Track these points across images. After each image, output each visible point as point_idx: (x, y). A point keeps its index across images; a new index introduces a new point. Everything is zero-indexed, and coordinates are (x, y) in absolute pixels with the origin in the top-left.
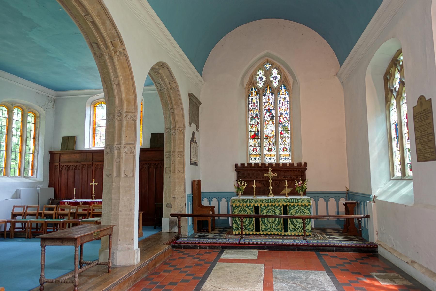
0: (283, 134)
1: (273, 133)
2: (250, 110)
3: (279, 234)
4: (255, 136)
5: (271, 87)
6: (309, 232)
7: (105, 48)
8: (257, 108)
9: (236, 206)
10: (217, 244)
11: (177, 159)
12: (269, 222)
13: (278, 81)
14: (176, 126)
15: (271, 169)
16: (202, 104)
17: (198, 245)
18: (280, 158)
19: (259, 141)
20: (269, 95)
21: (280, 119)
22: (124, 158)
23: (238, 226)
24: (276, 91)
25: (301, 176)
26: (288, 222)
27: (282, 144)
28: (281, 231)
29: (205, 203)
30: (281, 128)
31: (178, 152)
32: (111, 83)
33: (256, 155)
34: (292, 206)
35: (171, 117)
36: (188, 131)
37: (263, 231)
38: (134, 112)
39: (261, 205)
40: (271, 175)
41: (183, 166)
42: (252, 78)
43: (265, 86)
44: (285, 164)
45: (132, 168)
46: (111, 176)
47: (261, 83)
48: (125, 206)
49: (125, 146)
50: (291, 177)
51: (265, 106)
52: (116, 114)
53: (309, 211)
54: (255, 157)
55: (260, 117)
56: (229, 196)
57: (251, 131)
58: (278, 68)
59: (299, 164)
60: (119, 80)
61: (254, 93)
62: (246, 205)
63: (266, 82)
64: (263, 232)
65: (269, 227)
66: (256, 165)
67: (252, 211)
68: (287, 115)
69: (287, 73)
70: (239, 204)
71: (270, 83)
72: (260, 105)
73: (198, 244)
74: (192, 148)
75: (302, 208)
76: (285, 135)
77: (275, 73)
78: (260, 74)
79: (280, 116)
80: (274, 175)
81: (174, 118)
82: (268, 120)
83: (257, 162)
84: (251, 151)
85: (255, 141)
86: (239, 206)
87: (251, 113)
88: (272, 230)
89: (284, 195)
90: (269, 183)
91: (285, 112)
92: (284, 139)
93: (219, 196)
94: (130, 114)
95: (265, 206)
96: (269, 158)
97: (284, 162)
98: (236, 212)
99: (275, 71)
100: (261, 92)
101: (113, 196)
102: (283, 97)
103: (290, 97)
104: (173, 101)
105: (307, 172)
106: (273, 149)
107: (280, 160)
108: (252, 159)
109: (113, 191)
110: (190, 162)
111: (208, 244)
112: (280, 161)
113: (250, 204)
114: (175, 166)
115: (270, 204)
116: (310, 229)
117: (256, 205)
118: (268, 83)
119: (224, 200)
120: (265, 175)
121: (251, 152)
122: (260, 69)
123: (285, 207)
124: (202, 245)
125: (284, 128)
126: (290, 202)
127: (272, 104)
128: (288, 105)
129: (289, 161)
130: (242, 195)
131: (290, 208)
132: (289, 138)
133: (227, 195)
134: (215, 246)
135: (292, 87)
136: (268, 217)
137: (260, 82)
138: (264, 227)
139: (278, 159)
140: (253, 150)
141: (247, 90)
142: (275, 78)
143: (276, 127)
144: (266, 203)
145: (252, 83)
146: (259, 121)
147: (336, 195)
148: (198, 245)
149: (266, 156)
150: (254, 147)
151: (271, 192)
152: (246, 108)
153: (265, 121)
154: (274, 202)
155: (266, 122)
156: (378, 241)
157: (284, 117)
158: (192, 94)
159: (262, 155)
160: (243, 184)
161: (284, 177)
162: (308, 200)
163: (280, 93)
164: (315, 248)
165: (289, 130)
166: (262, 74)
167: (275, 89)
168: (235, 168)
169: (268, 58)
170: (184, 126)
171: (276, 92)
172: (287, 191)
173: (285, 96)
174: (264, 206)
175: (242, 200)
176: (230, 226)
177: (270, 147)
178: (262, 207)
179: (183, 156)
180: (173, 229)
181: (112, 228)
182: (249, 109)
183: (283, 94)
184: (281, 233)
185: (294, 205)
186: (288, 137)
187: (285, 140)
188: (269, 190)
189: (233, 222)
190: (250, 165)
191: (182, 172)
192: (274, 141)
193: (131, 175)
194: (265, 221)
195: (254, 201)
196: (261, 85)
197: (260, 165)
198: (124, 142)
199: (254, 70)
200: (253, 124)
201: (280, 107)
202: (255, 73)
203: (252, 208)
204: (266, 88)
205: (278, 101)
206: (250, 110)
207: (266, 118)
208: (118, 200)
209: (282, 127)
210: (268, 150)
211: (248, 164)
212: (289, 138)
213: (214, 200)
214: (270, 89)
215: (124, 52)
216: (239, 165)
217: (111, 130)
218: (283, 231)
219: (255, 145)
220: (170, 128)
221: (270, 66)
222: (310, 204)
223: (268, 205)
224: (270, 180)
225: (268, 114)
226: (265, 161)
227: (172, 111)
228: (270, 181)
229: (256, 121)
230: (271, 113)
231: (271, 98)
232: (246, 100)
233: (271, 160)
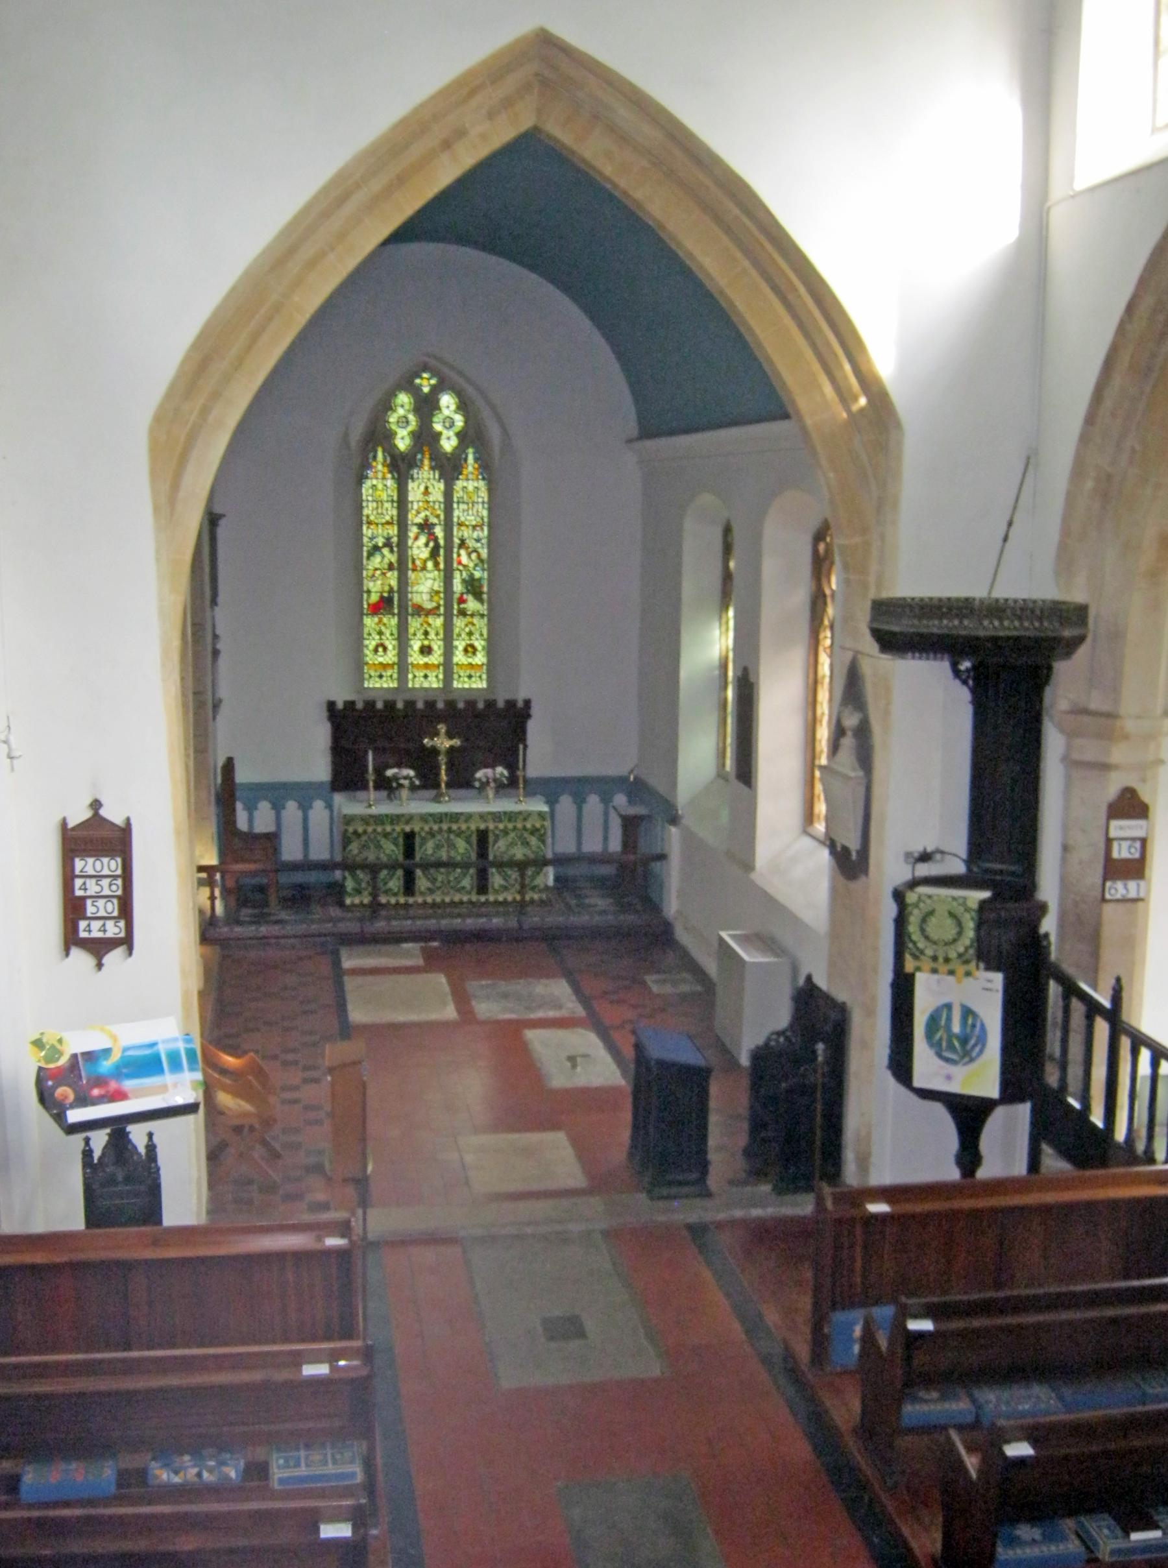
1: (436, 598)
4: (383, 605)
8: (388, 518)
9: (355, 833)
18: (456, 676)
19: (394, 621)
20: (429, 479)
21: (459, 555)
33: (385, 666)
37: (422, 893)
51: (414, 512)
59: (511, 704)
67: (396, 845)
68: (479, 545)
69: (486, 414)
85: (380, 621)
92: (469, 619)
93: (277, 793)
99: (447, 401)
100: (403, 466)
102: (470, 488)
103: (490, 491)
105: (532, 726)
106: (435, 647)
113: (393, 827)
115: (445, 826)
117: (408, 829)
118: (425, 438)
121: (370, 657)
123: (409, 837)
125: (472, 586)
127: (437, 507)
132: (482, 616)
140: (376, 651)
145: (378, 435)
147: (605, 786)
150: (379, 642)
153: (413, 561)
155: (418, 563)
157: (470, 550)
159: (448, 665)
166: (407, 407)
171: (449, 468)
173: (476, 484)
177: (426, 643)
185: (506, 827)
186: (481, 612)
187: (470, 620)
192: (438, 622)
196: (403, 443)
200: (376, 569)
202: (387, 406)
207: (415, 552)
209: (464, 581)
212: (482, 616)
213: (264, 807)
216: (340, 705)
219: (380, 633)
221: (433, 382)
230: (432, 537)
231: (434, 488)
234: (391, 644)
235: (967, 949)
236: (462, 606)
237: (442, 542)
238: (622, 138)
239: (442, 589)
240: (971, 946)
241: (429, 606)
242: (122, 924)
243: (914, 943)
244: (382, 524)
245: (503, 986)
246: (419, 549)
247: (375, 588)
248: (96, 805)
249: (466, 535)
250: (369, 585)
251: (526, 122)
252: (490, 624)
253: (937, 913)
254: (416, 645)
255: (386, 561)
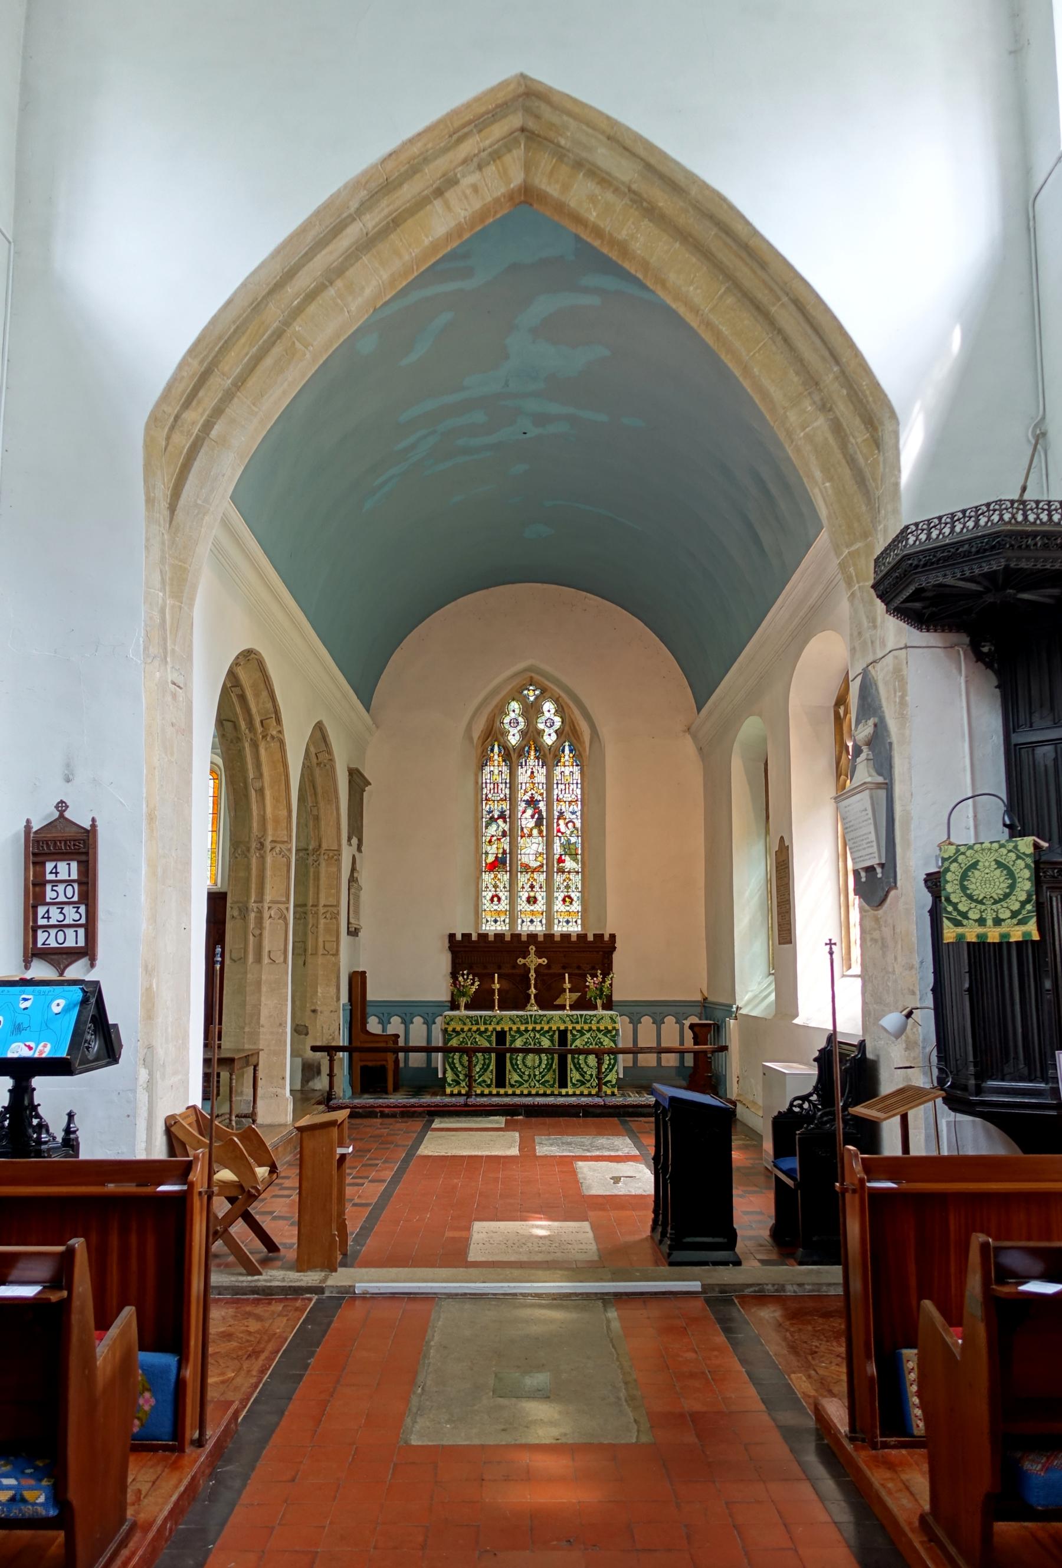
0: (563, 861)
1: (540, 859)
2: (486, 800)
3: (549, 1092)
5: (539, 744)
6: (613, 1086)
7: (247, 731)
8: (502, 796)
9: (454, 1030)
10: (418, 1107)
11: (322, 921)
12: (526, 1066)
13: (556, 732)
14: (320, 846)
15: (534, 949)
16: (370, 784)
17: (378, 1110)
18: (556, 921)
19: (507, 877)
20: (534, 766)
21: (558, 825)
22: (267, 928)
23: (458, 1076)
24: (550, 757)
25: (603, 964)
26: (569, 1066)
27: (562, 887)
28: (552, 1086)
29: (373, 1026)
30: (559, 848)
31: (325, 906)
32: (246, 787)
33: (498, 912)
34: (578, 1031)
35: (311, 824)
36: (347, 853)
37: (512, 1086)
38: (286, 842)
39: (510, 1029)
40: (533, 961)
41: (335, 939)
42: (493, 721)
43: (524, 743)
44: (566, 937)
45: (282, 947)
46: (243, 960)
47: (514, 735)
48: (270, 1016)
49: (270, 905)
50: (579, 968)
51: (522, 791)
52: (254, 845)
53: (614, 1042)
54: (495, 916)
55: (510, 817)
56: (431, 1010)
57: (487, 853)
58: (557, 701)
59: (599, 937)
60: (263, 782)
61: (496, 757)
62: (478, 1029)
63: (527, 733)
64: (513, 1089)
65: (526, 1078)
66: (499, 936)
68: (574, 816)
70: (462, 1026)
71: (537, 736)
72: (510, 788)
73: (377, 1107)
74: (351, 897)
75: (600, 1035)
76: (569, 864)
77: (549, 711)
78: (514, 711)
79: (559, 819)
80: (540, 961)
81: (317, 826)
82: (528, 825)
83: (499, 928)
84: (486, 902)
86: (462, 1030)
87: (488, 806)
88: (533, 1084)
89: (562, 1007)
90: (529, 980)
91: (571, 809)
92: (566, 875)
93: (407, 1010)
94: (278, 846)
95: (518, 1031)
96: (529, 920)
97: (565, 929)
98: (454, 1043)
99: (548, 707)
100: (514, 756)
101: (248, 998)
102: (567, 773)
104: (319, 791)
105: (616, 957)
106: (539, 898)
107: (556, 926)
108: (487, 921)
109: (248, 989)
110: (348, 928)
111: (399, 1107)
112: (556, 929)
114: (317, 939)
115: (530, 1027)
116: (614, 1081)
117: (499, 1028)
118: (531, 735)
119: (418, 1020)
120: (521, 961)
121: (486, 904)
122: (513, 700)
123: (563, 1034)
124: (387, 1110)
125: (569, 849)
126: (574, 1021)
127: (540, 787)
128: (579, 791)
129: (576, 929)
130: (468, 1007)
131: (574, 1035)
132: (577, 872)
133: (429, 1011)
134: (415, 1112)
135: (587, 749)
136: (526, 1051)
137: (513, 731)
138: (516, 1077)
139: (550, 923)
140: (492, 900)
141: (480, 751)
142: (548, 724)
143: (549, 845)
144: (522, 1024)
145: (493, 734)
146: (507, 828)
147: (677, 1008)
148: (378, 1110)
149: (523, 916)
151: (533, 1001)
152: (476, 794)
153: (522, 829)
154: (539, 1021)
155: (525, 831)
156: (738, 1095)
158: (358, 770)
159: (512, 913)
160: (469, 982)
161: (564, 968)
162: (611, 1018)
163: (559, 761)
164: (618, 1111)
165: (580, 852)
166: (517, 711)
167: (547, 752)
168: (447, 945)
169: (533, 675)
170: (340, 845)
171: (550, 758)
172: (568, 998)
173: (571, 769)
174: (516, 1032)
175: (468, 1017)
176: (440, 1075)
177: (532, 894)
178: (512, 1033)
179: (336, 916)
180: (311, 1084)
181: (258, 1053)
182: (484, 796)
183: (567, 763)
184: (552, 1089)
188: (529, 996)
189: (447, 1067)
190: (483, 936)
191: (334, 952)
192: (542, 877)
193: (282, 959)
194: (518, 1065)
195: (494, 1020)
196: (514, 739)
197: (508, 938)
198: (268, 898)
199: (498, 703)
200: (493, 836)
201: (558, 796)
202: (501, 710)
203: (489, 1036)
204: (527, 748)
205: (555, 782)
206: (486, 800)
208: (257, 1006)
209: (562, 845)
210: (528, 900)
211: (480, 935)
212: (577, 872)
213: (396, 1020)
214: (536, 750)
215: (280, 736)
216: (459, 937)
217: (242, 874)
218: (557, 1085)
219: (496, 886)
220: (306, 850)
221: (537, 692)
222: (615, 1025)
223: (526, 1028)
224: (532, 973)
225: (530, 812)
226: (520, 926)
227: (315, 813)
228: (532, 975)
229: (500, 828)
232: (476, 775)
233: (532, 925)
234: (504, 895)
235: (1023, 904)
236: (561, 865)
237: (544, 814)
238: (604, 179)
239: (545, 852)
240: (1028, 901)
241: (534, 864)
242: (82, 909)
243: (955, 906)
244: (498, 801)
245: (569, 1139)
246: (527, 821)
247: (492, 852)
248: (62, 806)
249: (564, 810)
250: (487, 848)
251: (517, 179)
252: (583, 880)
253: (980, 866)
254: (524, 895)
255: (501, 829)
